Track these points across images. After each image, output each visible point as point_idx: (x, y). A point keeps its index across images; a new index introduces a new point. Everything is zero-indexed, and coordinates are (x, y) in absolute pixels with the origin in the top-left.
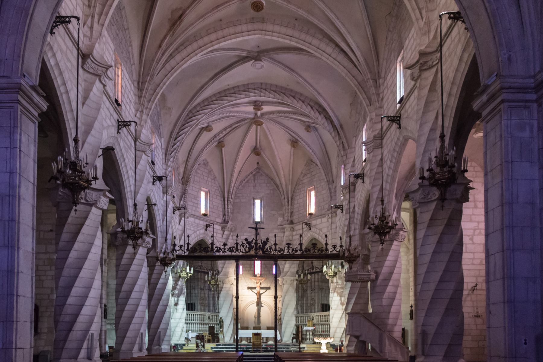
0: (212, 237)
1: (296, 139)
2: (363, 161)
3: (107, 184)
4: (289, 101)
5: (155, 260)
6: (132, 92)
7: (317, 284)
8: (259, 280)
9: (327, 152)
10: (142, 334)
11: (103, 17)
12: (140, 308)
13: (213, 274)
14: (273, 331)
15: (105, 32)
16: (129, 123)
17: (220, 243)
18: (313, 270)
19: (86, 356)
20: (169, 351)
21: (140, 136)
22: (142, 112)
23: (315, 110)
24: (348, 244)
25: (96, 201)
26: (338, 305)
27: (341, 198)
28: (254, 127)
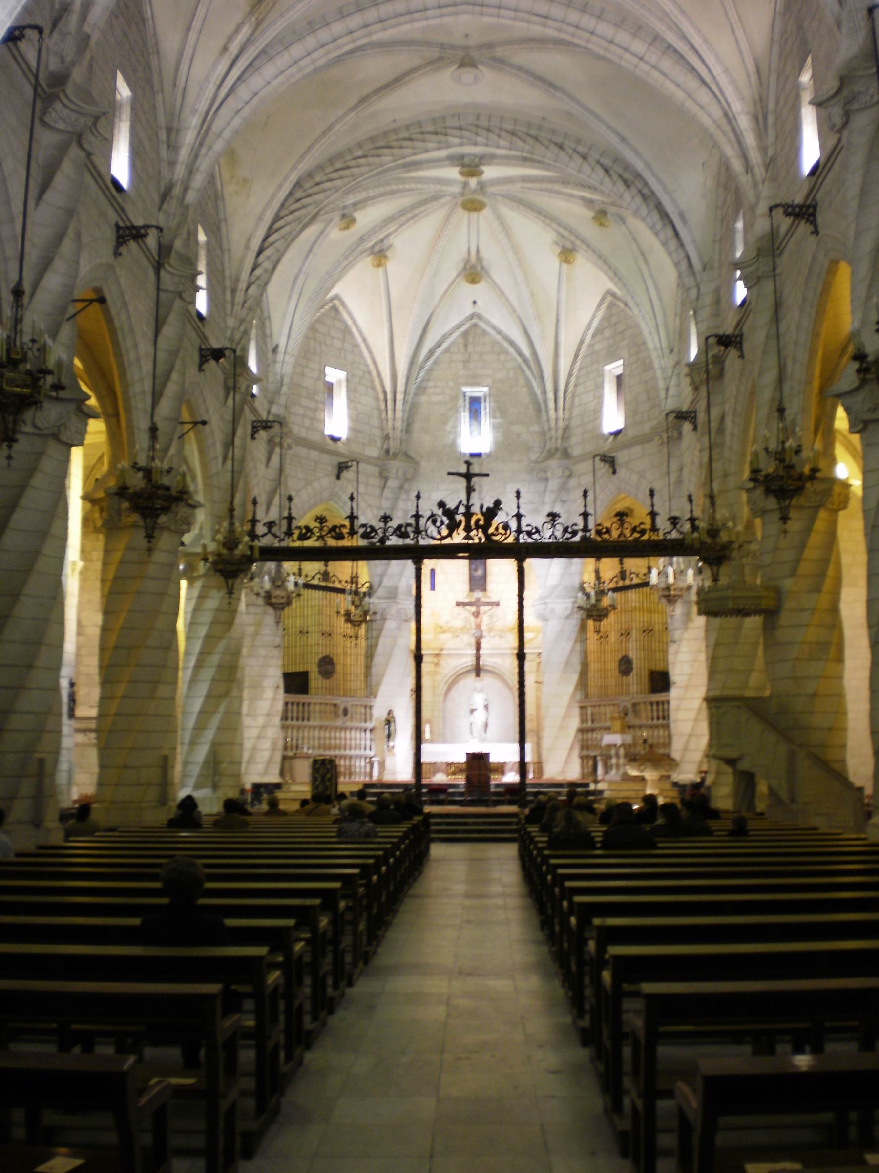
23: (615, 177)
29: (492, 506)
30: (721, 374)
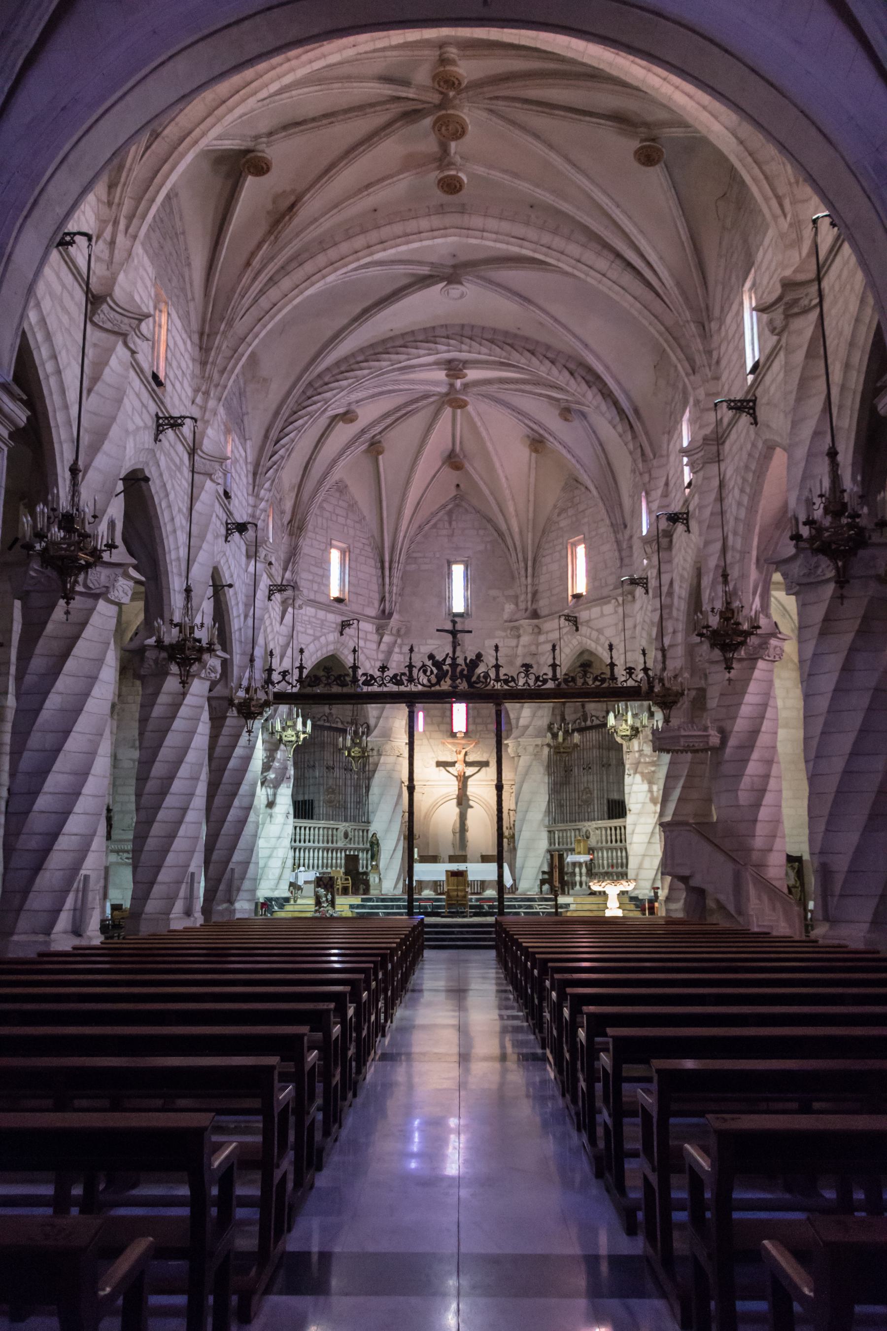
0: (354, 651)
1: (541, 435)
2: (686, 484)
3: (131, 553)
4: (523, 360)
5: (226, 704)
6: (187, 356)
7: (595, 752)
8: (464, 744)
9: (609, 464)
10: (193, 874)
11: (135, 221)
12: (191, 816)
13: (356, 732)
14: (494, 866)
15: (138, 249)
16: (179, 421)
17: (373, 663)
18: (585, 720)
19: (69, 928)
20: (252, 916)
21: (201, 443)
22: (207, 393)
24: (660, 666)
25: (107, 587)
26: (644, 803)
27: (643, 564)
28: (448, 411)
29: (474, 658)
30: (670, 547)
